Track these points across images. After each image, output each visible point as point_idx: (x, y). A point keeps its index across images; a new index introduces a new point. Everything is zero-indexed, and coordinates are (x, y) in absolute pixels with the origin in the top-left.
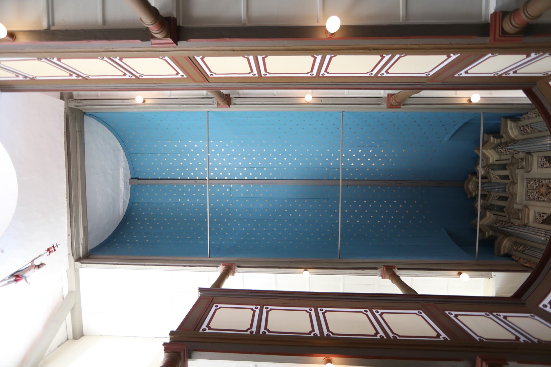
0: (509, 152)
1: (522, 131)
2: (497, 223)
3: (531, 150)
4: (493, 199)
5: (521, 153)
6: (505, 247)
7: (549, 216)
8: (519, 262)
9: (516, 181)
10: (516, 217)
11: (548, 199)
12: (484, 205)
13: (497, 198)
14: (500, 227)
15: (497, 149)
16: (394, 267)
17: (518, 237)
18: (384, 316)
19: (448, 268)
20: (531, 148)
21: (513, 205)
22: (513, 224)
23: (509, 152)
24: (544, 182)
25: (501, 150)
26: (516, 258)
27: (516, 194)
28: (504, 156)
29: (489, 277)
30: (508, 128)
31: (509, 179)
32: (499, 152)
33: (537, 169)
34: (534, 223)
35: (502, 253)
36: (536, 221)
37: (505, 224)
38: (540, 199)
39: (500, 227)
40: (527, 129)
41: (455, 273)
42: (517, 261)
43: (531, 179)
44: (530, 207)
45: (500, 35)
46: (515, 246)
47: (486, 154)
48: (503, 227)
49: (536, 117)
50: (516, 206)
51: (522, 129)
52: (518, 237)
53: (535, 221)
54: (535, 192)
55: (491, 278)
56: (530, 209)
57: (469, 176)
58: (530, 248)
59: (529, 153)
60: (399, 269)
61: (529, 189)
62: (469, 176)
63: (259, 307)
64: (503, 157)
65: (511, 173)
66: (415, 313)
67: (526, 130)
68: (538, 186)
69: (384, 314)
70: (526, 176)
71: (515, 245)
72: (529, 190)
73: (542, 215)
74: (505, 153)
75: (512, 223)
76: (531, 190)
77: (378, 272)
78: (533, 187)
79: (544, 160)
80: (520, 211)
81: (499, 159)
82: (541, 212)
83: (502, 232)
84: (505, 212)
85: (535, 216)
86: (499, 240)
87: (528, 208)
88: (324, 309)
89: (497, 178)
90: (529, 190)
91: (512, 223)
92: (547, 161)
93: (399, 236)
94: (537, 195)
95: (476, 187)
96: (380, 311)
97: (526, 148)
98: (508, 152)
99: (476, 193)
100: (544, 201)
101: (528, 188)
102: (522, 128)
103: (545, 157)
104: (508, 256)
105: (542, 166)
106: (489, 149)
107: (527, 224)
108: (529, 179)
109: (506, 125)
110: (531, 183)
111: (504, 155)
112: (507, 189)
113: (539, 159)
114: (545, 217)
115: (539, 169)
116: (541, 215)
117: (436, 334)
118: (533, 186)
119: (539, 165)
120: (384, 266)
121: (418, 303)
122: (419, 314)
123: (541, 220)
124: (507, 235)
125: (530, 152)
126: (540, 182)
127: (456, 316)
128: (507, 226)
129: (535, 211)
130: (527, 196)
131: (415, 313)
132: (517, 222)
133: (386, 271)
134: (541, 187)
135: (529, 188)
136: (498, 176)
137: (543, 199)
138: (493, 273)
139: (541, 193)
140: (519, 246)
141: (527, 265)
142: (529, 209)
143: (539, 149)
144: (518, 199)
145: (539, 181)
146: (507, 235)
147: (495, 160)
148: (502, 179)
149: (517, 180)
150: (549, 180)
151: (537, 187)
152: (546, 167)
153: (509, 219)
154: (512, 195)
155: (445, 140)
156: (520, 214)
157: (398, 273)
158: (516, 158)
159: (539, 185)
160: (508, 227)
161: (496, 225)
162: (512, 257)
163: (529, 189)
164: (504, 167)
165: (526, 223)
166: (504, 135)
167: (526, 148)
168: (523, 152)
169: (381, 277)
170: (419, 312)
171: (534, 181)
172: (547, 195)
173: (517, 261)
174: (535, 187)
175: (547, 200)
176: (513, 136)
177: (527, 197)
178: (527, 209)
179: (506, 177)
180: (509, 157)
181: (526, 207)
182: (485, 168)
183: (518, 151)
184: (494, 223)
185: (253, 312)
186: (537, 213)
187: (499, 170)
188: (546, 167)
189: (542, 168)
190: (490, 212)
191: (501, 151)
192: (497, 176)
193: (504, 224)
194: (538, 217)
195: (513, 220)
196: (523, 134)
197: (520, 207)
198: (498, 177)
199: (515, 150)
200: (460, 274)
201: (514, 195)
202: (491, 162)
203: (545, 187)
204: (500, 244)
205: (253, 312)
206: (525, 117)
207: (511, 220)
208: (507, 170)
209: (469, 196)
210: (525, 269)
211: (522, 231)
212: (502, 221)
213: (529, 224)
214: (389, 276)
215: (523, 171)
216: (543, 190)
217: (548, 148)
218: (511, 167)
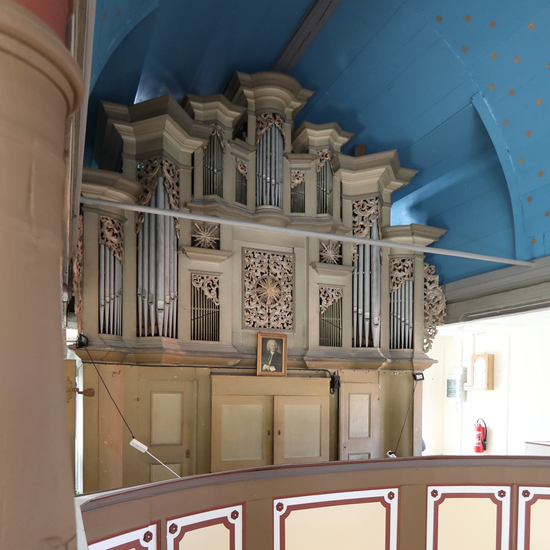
4: (238, 159)
13: (242, 171)
36: (196, 276)
40: (403, 274)
46: (113, 222)
51: (408, 264)
57: (308, 94)
61: (269, 258)
71: (115, 221)
72: (266, 256)
73: (214, 289)
76: (269, 262)
81: (344, 192)
82: (221, 287)
88: (238, 523)
90: (266, 256)
94: (258, 274)
95: (275, 111)
99: (250, 98)
100: (244, 289)
102: (408, 263)
105: (324, 294)
106: (379, 181)
108: (294, 258)
109: (347, 137)
113: (337, 289)
114: (209, 296)
115: (317, 287)
119: (327, 288)
129: (220, 273)
135: (271, 257)
140: (116, 231)
150: (291, 301)
151: (276, 275)
159: (279, 279)
163: (269, 258)
182: (326, 151)
184: (170, 162)
185: (168, 522)
186: (216, 278)
190: (202, 147)
198: (297, 182)
202: (308, 131)
205: (168, 522)
209: (242, 76)
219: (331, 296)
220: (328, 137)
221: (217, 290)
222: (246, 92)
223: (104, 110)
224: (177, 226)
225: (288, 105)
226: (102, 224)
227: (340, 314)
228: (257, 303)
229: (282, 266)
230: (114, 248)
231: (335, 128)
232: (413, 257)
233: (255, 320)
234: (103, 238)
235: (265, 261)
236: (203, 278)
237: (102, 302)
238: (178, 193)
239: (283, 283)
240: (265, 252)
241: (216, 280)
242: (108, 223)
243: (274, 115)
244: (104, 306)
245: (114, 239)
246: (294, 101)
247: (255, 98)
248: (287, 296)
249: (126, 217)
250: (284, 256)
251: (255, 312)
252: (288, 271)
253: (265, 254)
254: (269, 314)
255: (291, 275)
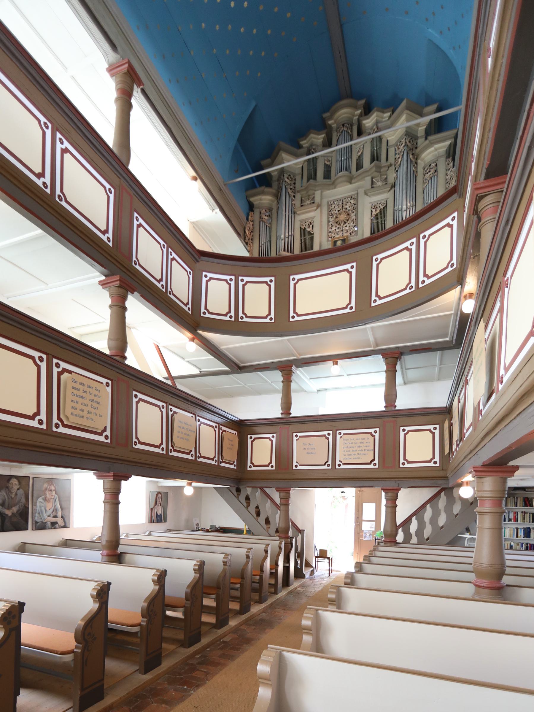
0: (399, 158)
1: (430, 165)
2: (291, 178)
3: (397, 188)
5: (395, 175)
6: (261, 200)
7: (311, 233)
8: (248, 222)
9: (353, 181)
10: (303, 198)
11: (332, 225)
12: (314, 147)
14: (286, 184)
15: (405, 138)
16: (140, 83)
17: (278, 209)
18: (67, 156)
19: (193, 161)
20: (401, 188)
21: (318, 190)
22: (293, 198)
23: (399, 158)
24: (353, 214)
25: (403, 145)
26: (252, 217)
27: (335, 188)
28: (394, 151)
29: (211, 208)
30: (437, 144)
31: (357, 170)
32: (400, 142)
33: (370, 203)
34: (299, 221)
35: (252, 199)
37: (291, 189)
38: (330, 217)
39: (285, 185)
40: (429, 174)
41: (193, 173)
42: (247, 219)
43: (357, 199)
44: (319, 210)
45: (478, 195)
47: (398, 122)
48: (286, 188)
49: (446, 180)
50: (318, 194)
52: (278, 209)
53: (301, 221)
54: (339, 209)
55: (211, 210)
56: (316, 211)
58: (268, 227)
59: (394, 186)
60: (143, 91)
61: (343, 201)
62: (362, 102)
63: (109, 441)
64: (392, 151)
65: (366, 171)
66: (105, 188)
67: (430, 172)
68: (347, 210)
69: (68, 154)
70: (361, 192)
71: (267, 210)
72: (341, 201)
73: (311, 226)
74: (397, 152)
75: (294, 197)
76: (343, 204)
77: (113, 56)
78: (346, 205)
79: (382, 207)
80: (313, 200)
83: (279, 189)
84: (308, 183)
85: (308, 219)
86: (267, 190)
87: (317, 208)
89: (358, 152)
90: (341, 201)
91: (294, 197)
92: (380, 210)
93: (203, 25)
94: (337, 212)
96: (66, 144)
97: (401, 180)
98: (398, 156)
101: (345, 199)
103: (385, 207)
104: (251, 207)
107: (297, 213)
110: (352, 201)
111: (395, 150)
112: (340, 174)
114: (308, 230)
116: (311, 224)
117: (105, 228)
118: (347, 204)
119: (376, 203)
120: (129, 63)
121: (120, 178)
122: (108, 192)
123: (304, 226)
124: (277, 196)
125: (395, 187)
126: (353, 211)
127: (140, 225)
128: (289, 193)
130: (334, 202)
131: (105, 188)
132: (297, 202)
133: (125, 73)
134: (346, 213)
135: (344, 200)
136: (362, 153)
137: (331, 220)
138: (218, 210)
139: (338, 216)
141: (247, 232)
142: (316, 210)
143: (398, 196)
144: (327, 193)
145: (354, 209)
146: (277, 196)
147: (389, 139)
148: (357, 160)
149: (355, 183)
151: (346, 209)
152: (372, 211)
153: (299, 192)
154: (333, 183)
155: (430, 30)
156: (308, 202)
157: (137, 94)
158: (388, 171)
159: (349, 210)
160: (287, 194)
161: (288, 178)
162: (251, 213)
163: (343, 201)
164: (376, 157)
165: (298, 212)
166: (427, 141)
167: (401, 180)
168: (396, 178)
169: (107, 66)
170: (110, 189)
171: (354, 204)
172: (336, 223)
173: (247, 219)
174: (346, 207)
175: (330, 225)
176: (423, 155)
177: (332, 202)
178: (315, 208)
179: (359, 166)
180: (391, 160)
181: (319, 206)
183: (399, 171)
184: (289, 174)
187: (371, 150)
188: (372, 211)
189: (371, 207)
191: (402, 144)
192: (361, 151)
193: (291, 187)
194: (308, 223)
195: (298, 196)
196: (424, 169)
197: (317, 199)
198: (360, 153)
199: (400, 166)
200: (195, 179)
201: (334, 185)
203: (346, 218)
204: (263, 193)
206: (449, 165)
207: (299, 194)
208: (371, 163)
209: (325, 115)
210: (242, 234)
211: (285, 212)
212: (295, 184)
213: (296, 216)
214: (120, 87)
215: (369, 185)
216: (342, 217)
217: (397, 207)
218: (374, 169)
219: (378, 207)
220: (376, 118)
221: (313, 226)
222: (330, 122)
223: (477, 272)
224: (293, 202)
225: (354, 116)
226: (261, 213)
227: (385, 216)
228: (336, 227)
229: (351, 203)
230: (265, 221)
231: (378, 111)
232: (436, 159)
233: (334, 236)
234: (261, 218)
235: (340, 203)
236: (306, 222)
237: (261, 244)
238: (295, 187)
239: (351, 212)
240: (340, 199)
241: (312, 221)
242: (263, 212)
243: (343, 125)
244: (262, 246)
245: (266, 218)
246: (356, 111)
247: (335, 122)
248: (353, 218)
249: (273, 208)
250: (351, 197)
251: (335, 231)
252: (354, 204)
253: (340, 200)
254: (342, 230)
255: (355, 206)
